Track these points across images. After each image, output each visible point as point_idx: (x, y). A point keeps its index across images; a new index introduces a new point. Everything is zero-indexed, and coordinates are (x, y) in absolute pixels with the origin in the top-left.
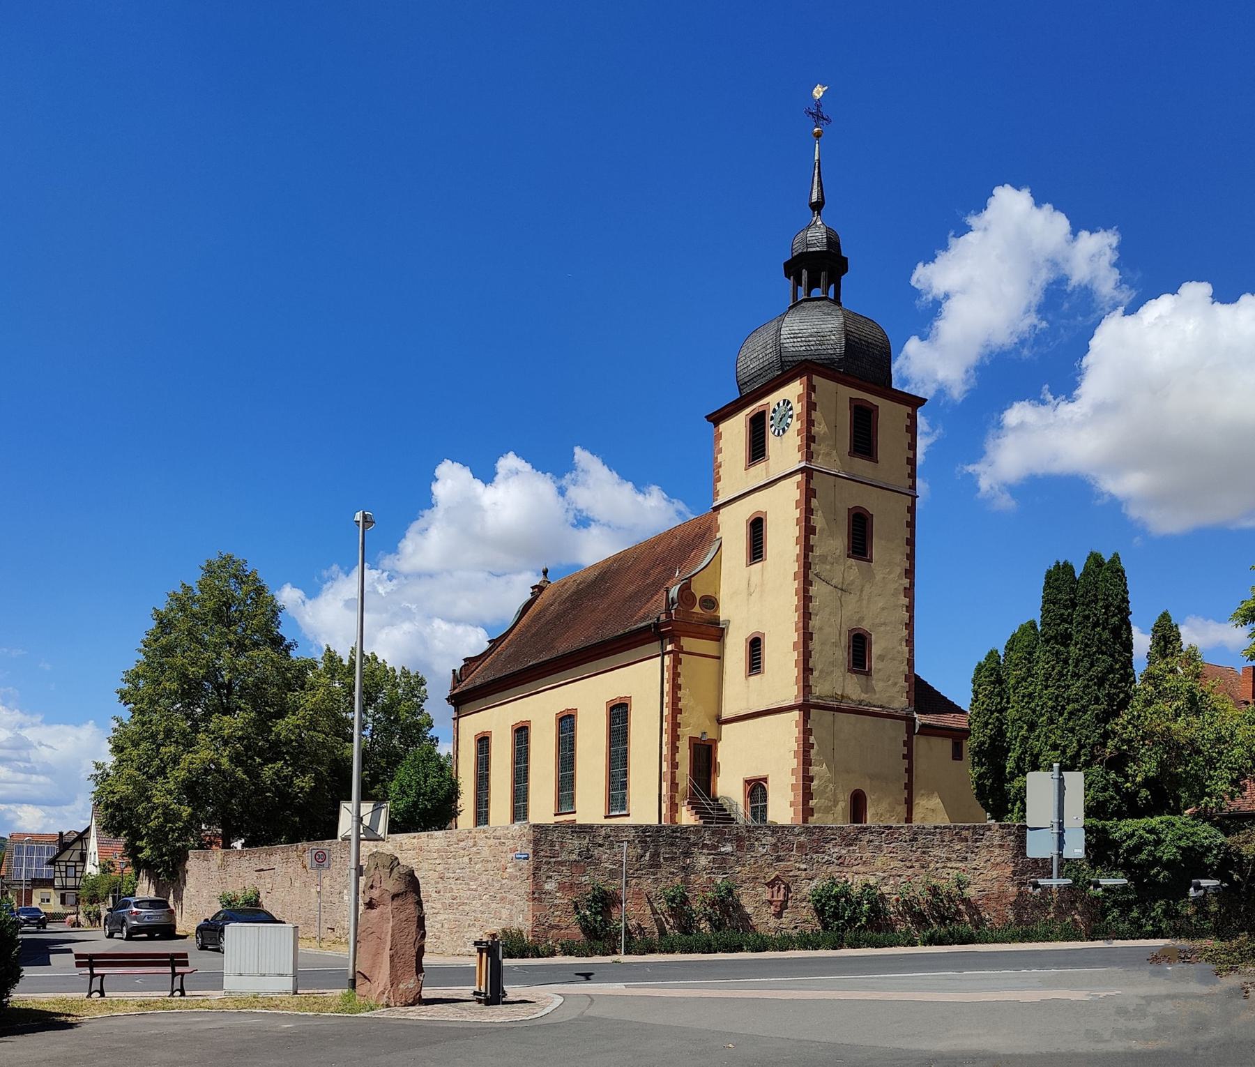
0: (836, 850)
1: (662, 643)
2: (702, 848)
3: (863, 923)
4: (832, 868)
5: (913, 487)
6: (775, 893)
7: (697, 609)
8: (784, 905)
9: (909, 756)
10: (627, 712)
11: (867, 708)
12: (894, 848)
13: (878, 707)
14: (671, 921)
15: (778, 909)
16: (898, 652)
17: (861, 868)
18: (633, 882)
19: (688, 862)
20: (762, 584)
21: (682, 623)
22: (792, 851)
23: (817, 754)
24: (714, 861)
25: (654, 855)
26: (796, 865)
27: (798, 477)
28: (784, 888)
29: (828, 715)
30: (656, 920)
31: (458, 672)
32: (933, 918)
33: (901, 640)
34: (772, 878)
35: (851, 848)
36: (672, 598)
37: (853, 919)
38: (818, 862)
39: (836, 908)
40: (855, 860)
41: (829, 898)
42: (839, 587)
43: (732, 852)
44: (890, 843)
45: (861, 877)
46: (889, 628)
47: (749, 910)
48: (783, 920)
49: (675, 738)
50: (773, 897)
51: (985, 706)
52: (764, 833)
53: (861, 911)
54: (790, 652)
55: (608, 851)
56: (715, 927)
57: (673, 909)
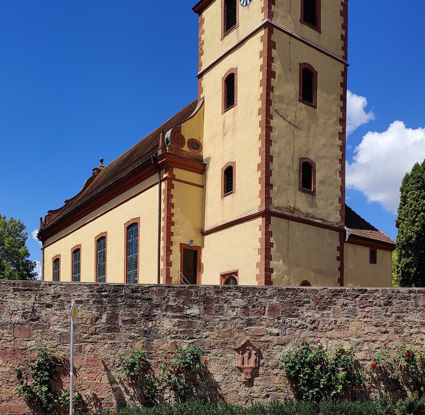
0: (310, 314)
1: (160, 173)
2: (166, 310)
3: (339, 391)
4: (307, 333)
5: (345, 57)
6: (246, 360)
7: (186, 148)
8: (255, 373)
9: (341, 259)
10: (137, 229)
11: (312, 219)
12: (368, 312)
13: (320, 219)
14: (131, 390)
15: (249, 377)
16: (334, 180)
17: (335, 334)
18: (88, 347)
19: (150, 325)
20: (234, 124)
21: (174, 157)
22: (264, 314)
23: (276, 251)
24: (179, 324)
25: (111, 317)
26: (267, 329)
27: (262, 33)
28: (255, 354)
29: (283, 222)
30: (114, 390)
31: (43, 219)
32: (408, 385)
33: (336, 171)
34: (243, 343)
35: (324, 312)
36: (167, 139)
37: (329, 387)
38: (290, 326)
39: (310, 375)
40: (330, 324)
41: (303, 365)
42: (293, 123)
43: (199, 315)
44: (364, 308)
45: (336, 342)
46: (328, 161)
47: (217, 378)
48: (255, 388)
49: (169, 243)
50: (243, 364)
51: (413, 207)
52: (234, 295)
53: (337, 379)
54: (255, 173)
55: (58, 313)
56: (181, 396)
57: (133, 378)
